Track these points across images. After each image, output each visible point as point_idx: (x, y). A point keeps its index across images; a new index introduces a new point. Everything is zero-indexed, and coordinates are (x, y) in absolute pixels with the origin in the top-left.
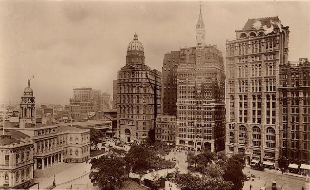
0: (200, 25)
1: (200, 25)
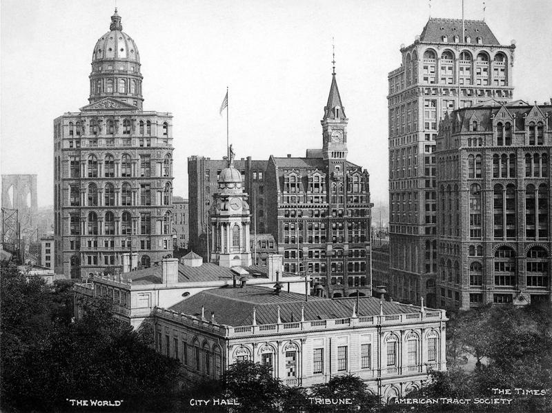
0: (116, 12)
1: (116, 12)
